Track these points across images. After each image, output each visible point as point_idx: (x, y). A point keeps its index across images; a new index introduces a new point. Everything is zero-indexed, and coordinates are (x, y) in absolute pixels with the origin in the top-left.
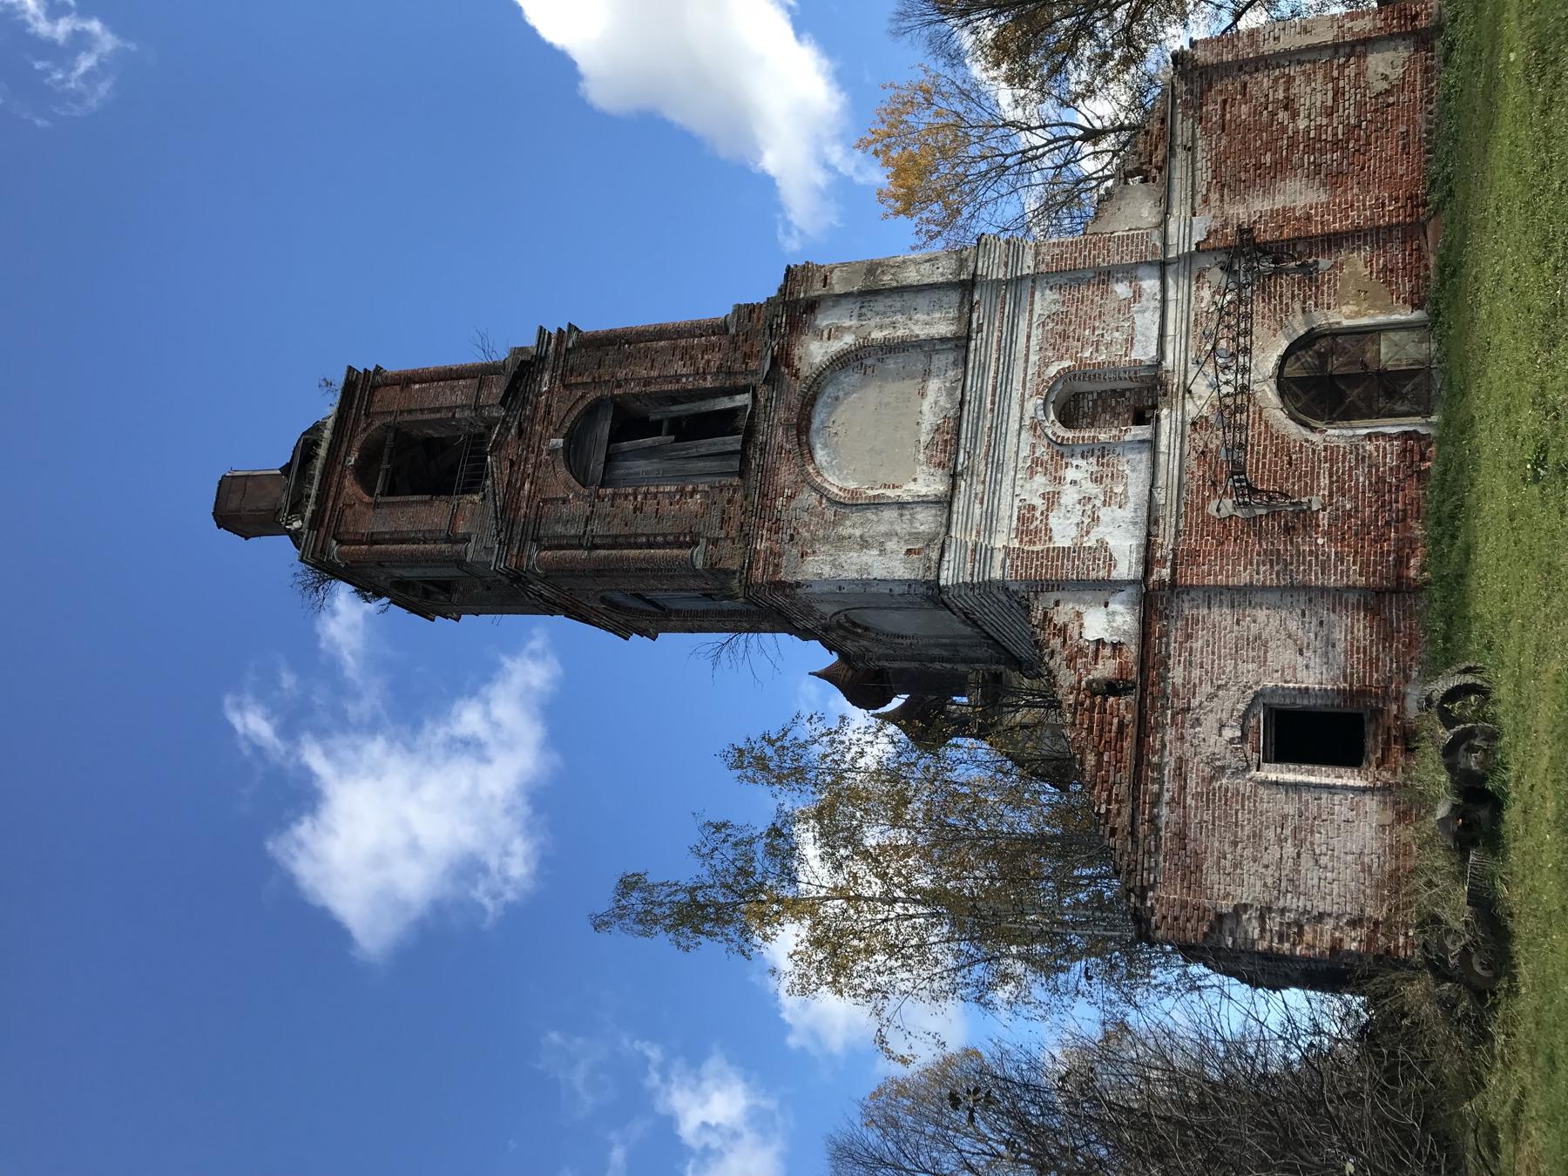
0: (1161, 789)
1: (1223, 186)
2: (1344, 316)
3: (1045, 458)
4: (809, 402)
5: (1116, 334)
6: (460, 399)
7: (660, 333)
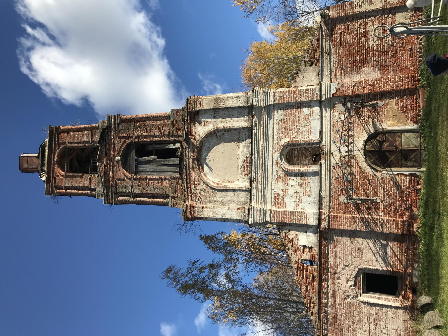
0: (328, 301)
1: (342, 69)
2: (388, 125)
3: (282, 176)
4: (200, 149)
5: (304, 129)
6: (86, 139)
7: (148, 119)
